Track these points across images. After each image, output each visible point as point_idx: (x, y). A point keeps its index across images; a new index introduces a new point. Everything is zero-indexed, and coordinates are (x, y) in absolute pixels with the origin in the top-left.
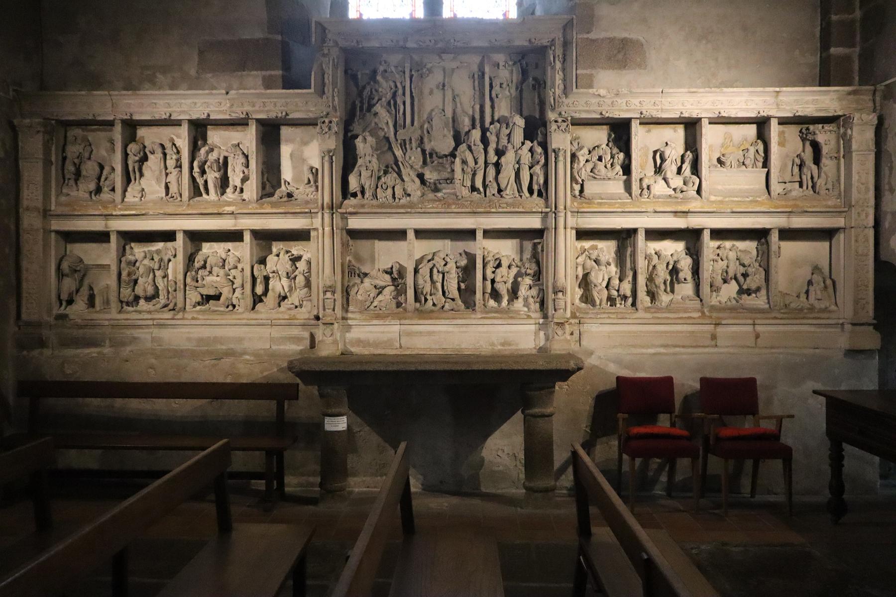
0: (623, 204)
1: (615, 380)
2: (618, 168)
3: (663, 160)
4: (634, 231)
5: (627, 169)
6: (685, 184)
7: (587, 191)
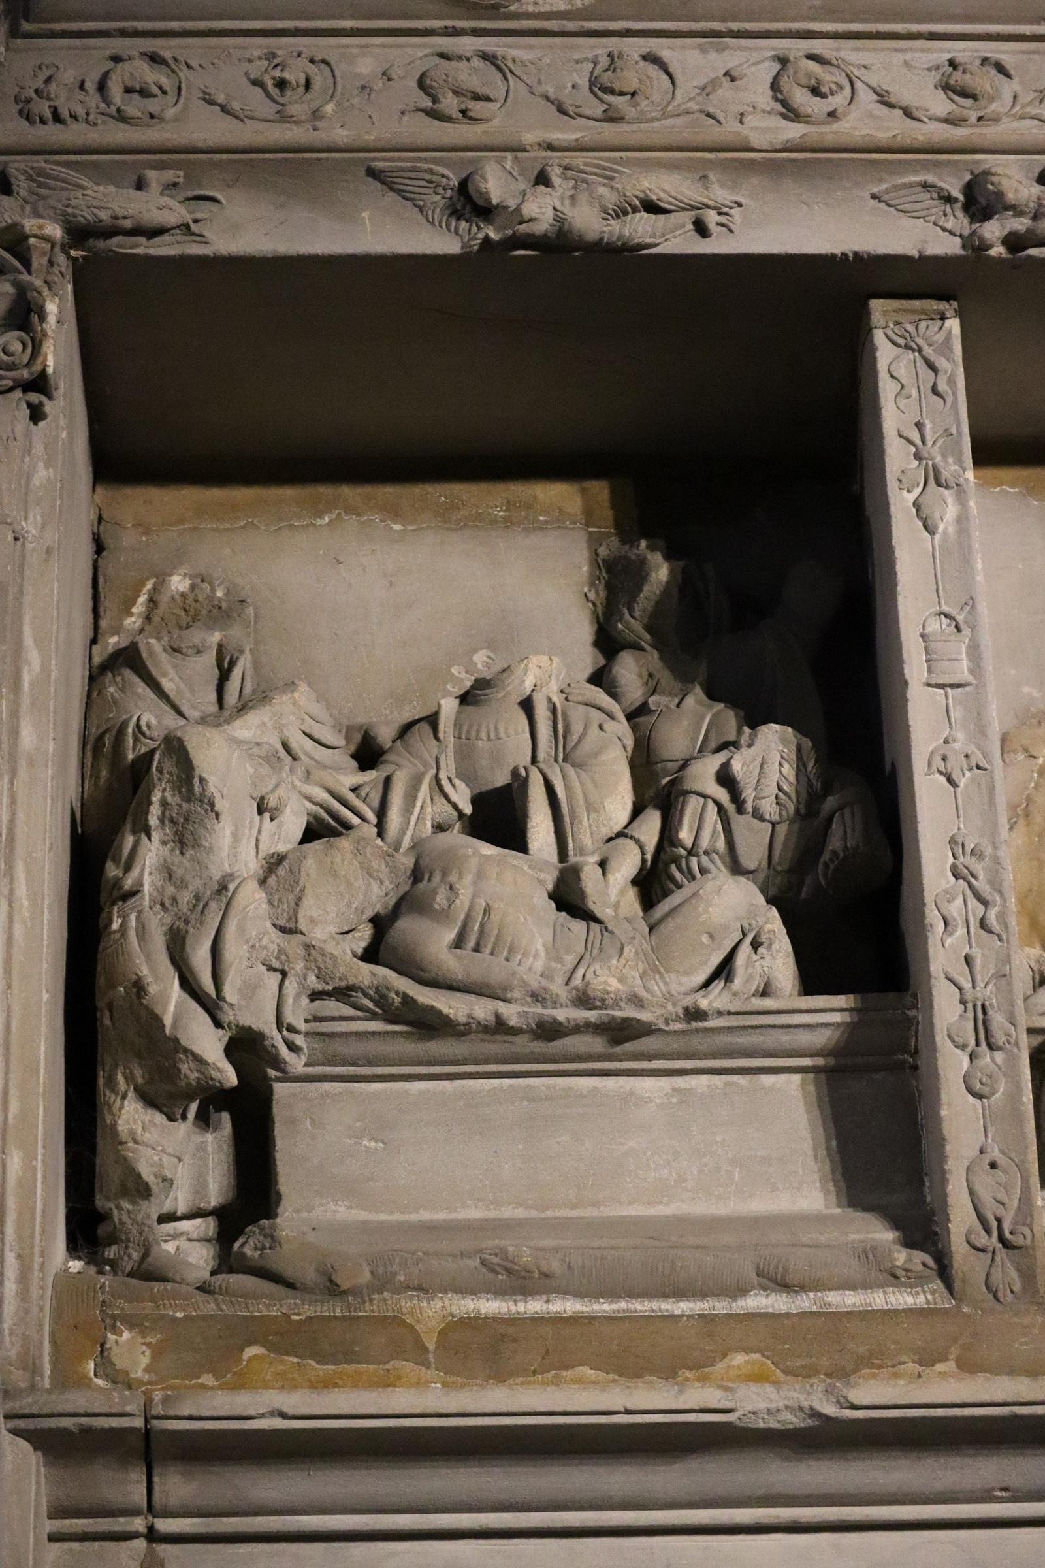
0: (833, 1344)
1: (100, 490)
2: (728, 900)
5: (853, 916)
7: (313, 1210)
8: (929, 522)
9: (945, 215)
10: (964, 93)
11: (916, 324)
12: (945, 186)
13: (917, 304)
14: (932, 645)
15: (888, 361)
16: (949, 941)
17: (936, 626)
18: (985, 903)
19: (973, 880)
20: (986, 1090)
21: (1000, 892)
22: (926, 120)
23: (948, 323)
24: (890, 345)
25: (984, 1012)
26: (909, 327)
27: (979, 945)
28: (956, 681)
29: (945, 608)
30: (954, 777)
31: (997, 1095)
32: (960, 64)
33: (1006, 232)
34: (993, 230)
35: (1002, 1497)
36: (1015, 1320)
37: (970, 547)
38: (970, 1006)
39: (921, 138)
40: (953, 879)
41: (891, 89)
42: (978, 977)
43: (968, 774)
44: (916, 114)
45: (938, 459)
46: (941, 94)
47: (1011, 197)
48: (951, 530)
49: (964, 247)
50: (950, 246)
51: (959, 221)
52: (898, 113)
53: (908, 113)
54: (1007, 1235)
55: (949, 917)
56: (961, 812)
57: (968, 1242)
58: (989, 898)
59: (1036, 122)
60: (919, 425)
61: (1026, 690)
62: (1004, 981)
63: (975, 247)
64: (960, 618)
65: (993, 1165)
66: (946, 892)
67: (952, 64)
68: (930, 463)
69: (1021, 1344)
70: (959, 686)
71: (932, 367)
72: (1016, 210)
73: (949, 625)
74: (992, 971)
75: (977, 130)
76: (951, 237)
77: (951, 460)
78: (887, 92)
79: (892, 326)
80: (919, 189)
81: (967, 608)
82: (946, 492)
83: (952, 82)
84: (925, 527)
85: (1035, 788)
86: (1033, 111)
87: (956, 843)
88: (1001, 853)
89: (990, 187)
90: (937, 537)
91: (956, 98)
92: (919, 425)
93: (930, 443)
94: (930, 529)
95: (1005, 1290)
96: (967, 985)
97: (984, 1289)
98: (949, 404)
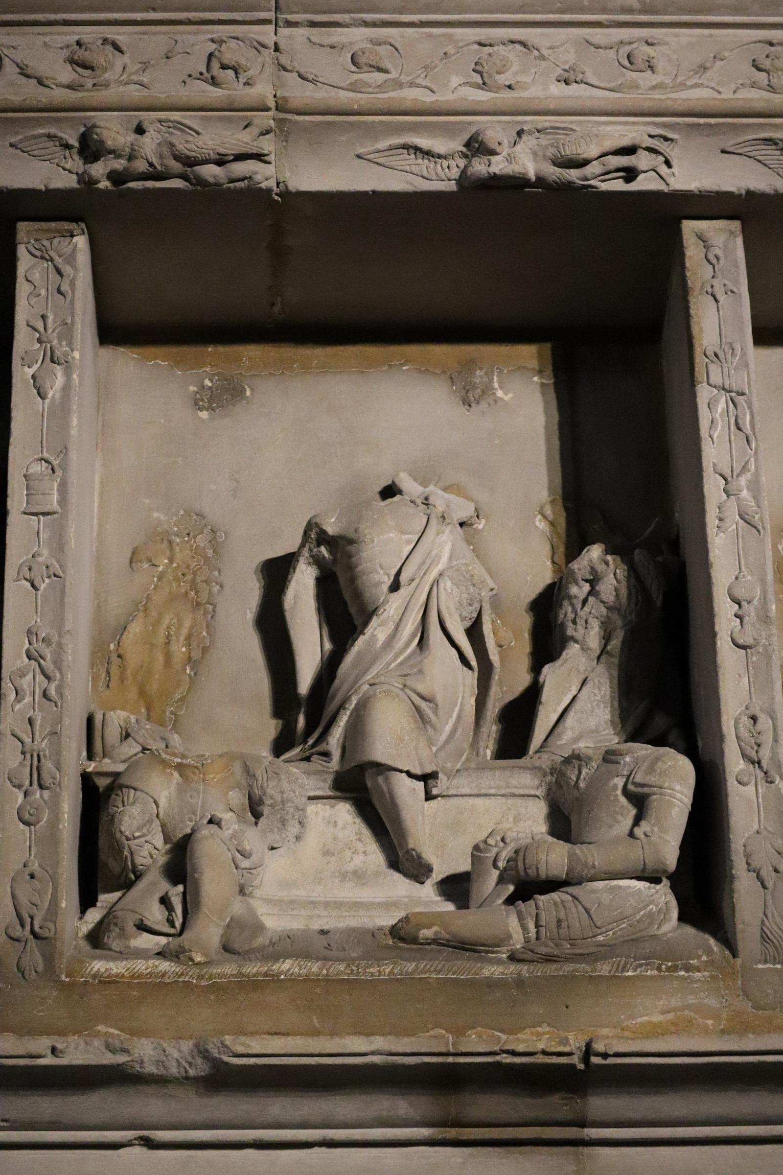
3: (344, 613)
4: (87, 779)
6: (563, 823)
8: (41, 391)
9: (65, 158)
10: (85, 67)
11: (51, 239)
12: (63, 135)
13: (53, 225)
14: (31, 483)
15: (26, 268)
16: (17, 707)
17: (37, 468)
18: (48, 678)
19: (42, 661)
20: (33, 819)
21: (60, 670)
22: (54, 86)
23: (75, 239)
24: (29, 256)
25: (39, 761)
26: (45, 243)
27: (41, 710)
28: (46, 510)
29: (46, 455)
30: (36, 583)
31: (41, 823)
32: (84, 44)
33: (108, 171)
34: (98, 169)
35: (4, 1127)
36: (36, 993)
37: (69, 409)
38: (28, 756)
39: (44, 100)
40: (27, 660)
41: (30, 64)
42: (37, 734)
43: (47, 581)
44: (47, 82)
45: (55, 342)
46: (68, 67)
47: (110, 143)
48: (58, 396)
49: (79, 182)
50: (70, 182)
51: (76, 163)
52: (33, 81)
53: (40, 82)
54: (37, 928)
55: (18, 688)
56: (39, 609)
57: (6, 934)
58: (51, 675)
59: (138, 86)
60: (44, 317)
61: (155, 515)
62: (55, 736)
63: (87, 182)
64: (55, 463)
65: (32, 876)
66: (19, 670)
67: (79, 43)
68: (49, 345)
69: (39, 1011)
70: (48, 514)
71: (59, 272)
72: (115, 153)
73: (47, 468)
74: (48, 730)
75: (92, 94)
76: (70, 175)
77: (64, 343)
78: (26, 66)
79: (33, 242)
80: (46, 139)
81: (62, 455)
82: (58, 367)
83: (76, 57)
84: (39, 394)
85: (154, 589)
86: (135, 78)
87: (31, 633)
88: (64, 641)
89: (95, 136)
90: (47, 401)
91: (79, 69)
92: (44, 317)
93: (50, 331)
94: (42, 395)
95: (30, 970)
96: (28, 740)
97: (16, 970)
98: (68, 300)
